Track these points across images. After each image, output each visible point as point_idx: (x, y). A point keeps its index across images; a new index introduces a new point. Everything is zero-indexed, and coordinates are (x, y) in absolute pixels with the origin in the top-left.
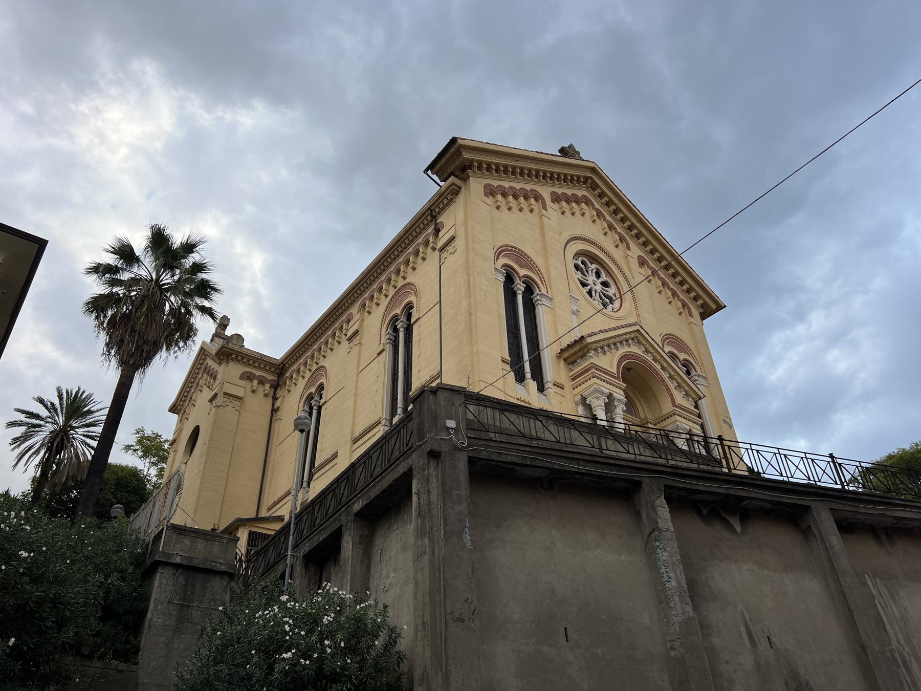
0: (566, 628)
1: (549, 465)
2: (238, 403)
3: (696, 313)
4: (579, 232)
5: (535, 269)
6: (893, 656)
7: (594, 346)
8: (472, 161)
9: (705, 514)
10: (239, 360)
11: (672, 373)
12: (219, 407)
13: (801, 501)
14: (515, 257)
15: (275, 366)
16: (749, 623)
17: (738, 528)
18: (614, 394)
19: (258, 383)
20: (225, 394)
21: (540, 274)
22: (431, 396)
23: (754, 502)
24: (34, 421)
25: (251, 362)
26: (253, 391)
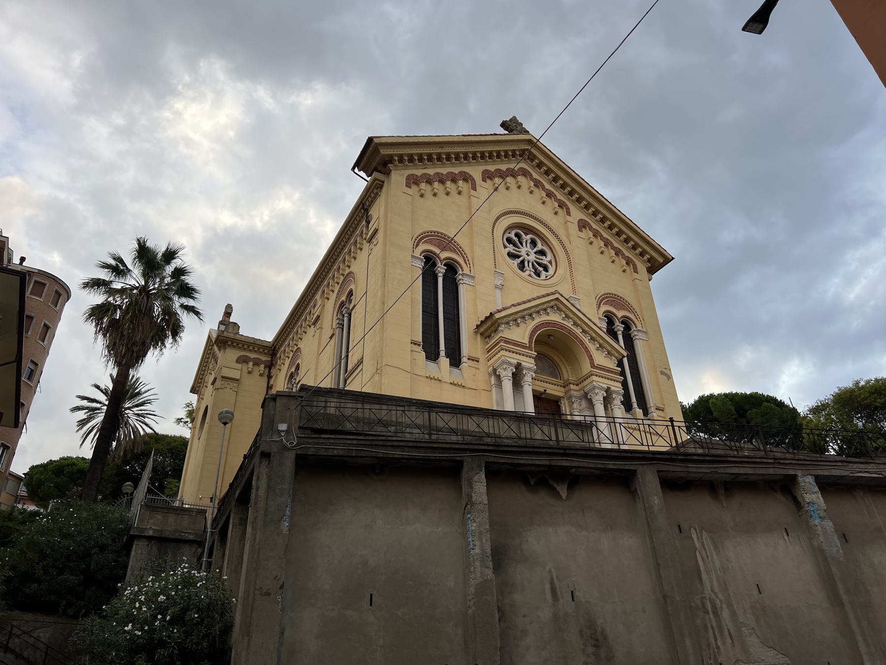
0: (371, 595)
1: (374, 454)
2: (235, 385)
3: (642, 268)
4: (511, 206)
5: (459, 250)
6: (703, 604)
7: (505, 320)
8: (391, 156)
10: (235, 346)
11: (594, 335)
12: (218, 389)
13: (628, 466)
14: (438, 241)
15: (268, 348)
16: (555, 581)
17: (564, 495)
18: (523, 364)
19: (253, 365)
20: (223, 377)
21: (464, 254)
22: (272, 403)
23: (580, 470)
24: (95, 405)
25: (246, 347)
26: (249, 373)
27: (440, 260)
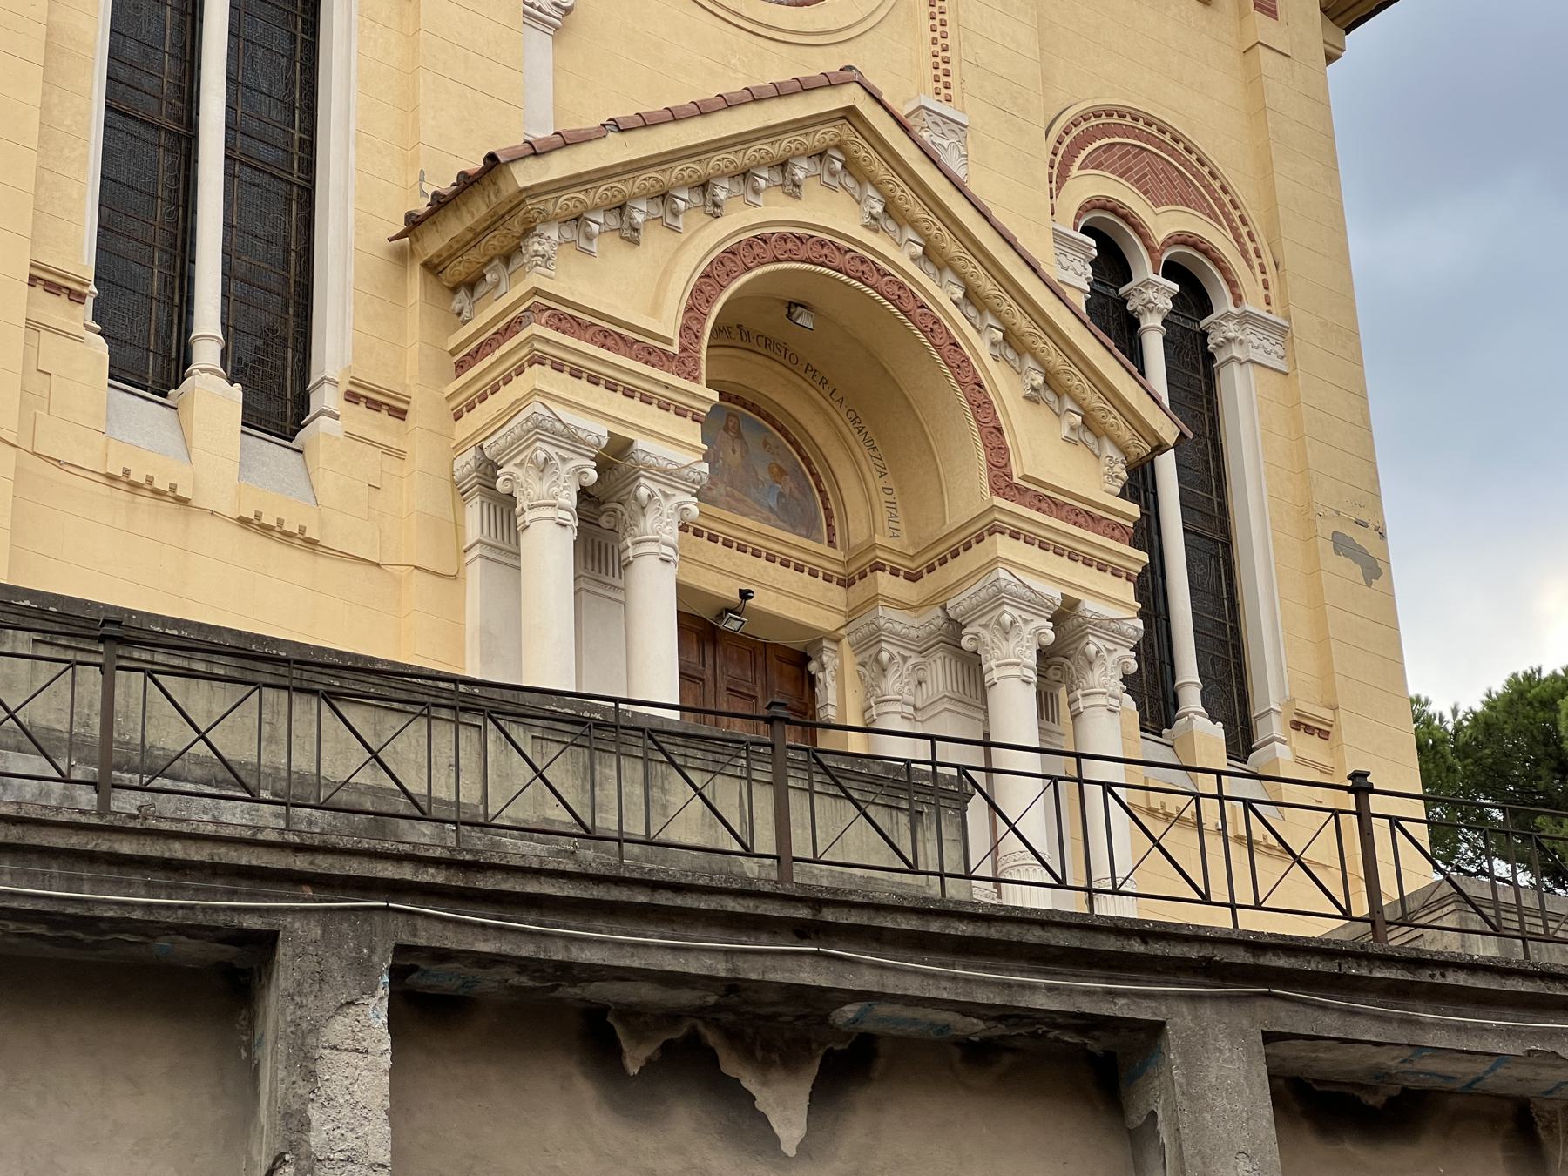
7: (565, 202)
9: (634, 1070)
11: (1022, 323)
13: (1121, 1001)
17: (790, 1125)
18: (642, 443)
23: (884, 1010)
27: (1147, 247)
